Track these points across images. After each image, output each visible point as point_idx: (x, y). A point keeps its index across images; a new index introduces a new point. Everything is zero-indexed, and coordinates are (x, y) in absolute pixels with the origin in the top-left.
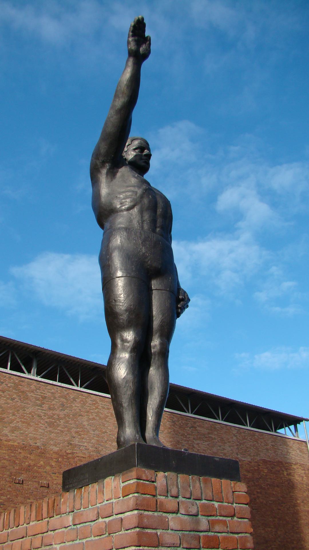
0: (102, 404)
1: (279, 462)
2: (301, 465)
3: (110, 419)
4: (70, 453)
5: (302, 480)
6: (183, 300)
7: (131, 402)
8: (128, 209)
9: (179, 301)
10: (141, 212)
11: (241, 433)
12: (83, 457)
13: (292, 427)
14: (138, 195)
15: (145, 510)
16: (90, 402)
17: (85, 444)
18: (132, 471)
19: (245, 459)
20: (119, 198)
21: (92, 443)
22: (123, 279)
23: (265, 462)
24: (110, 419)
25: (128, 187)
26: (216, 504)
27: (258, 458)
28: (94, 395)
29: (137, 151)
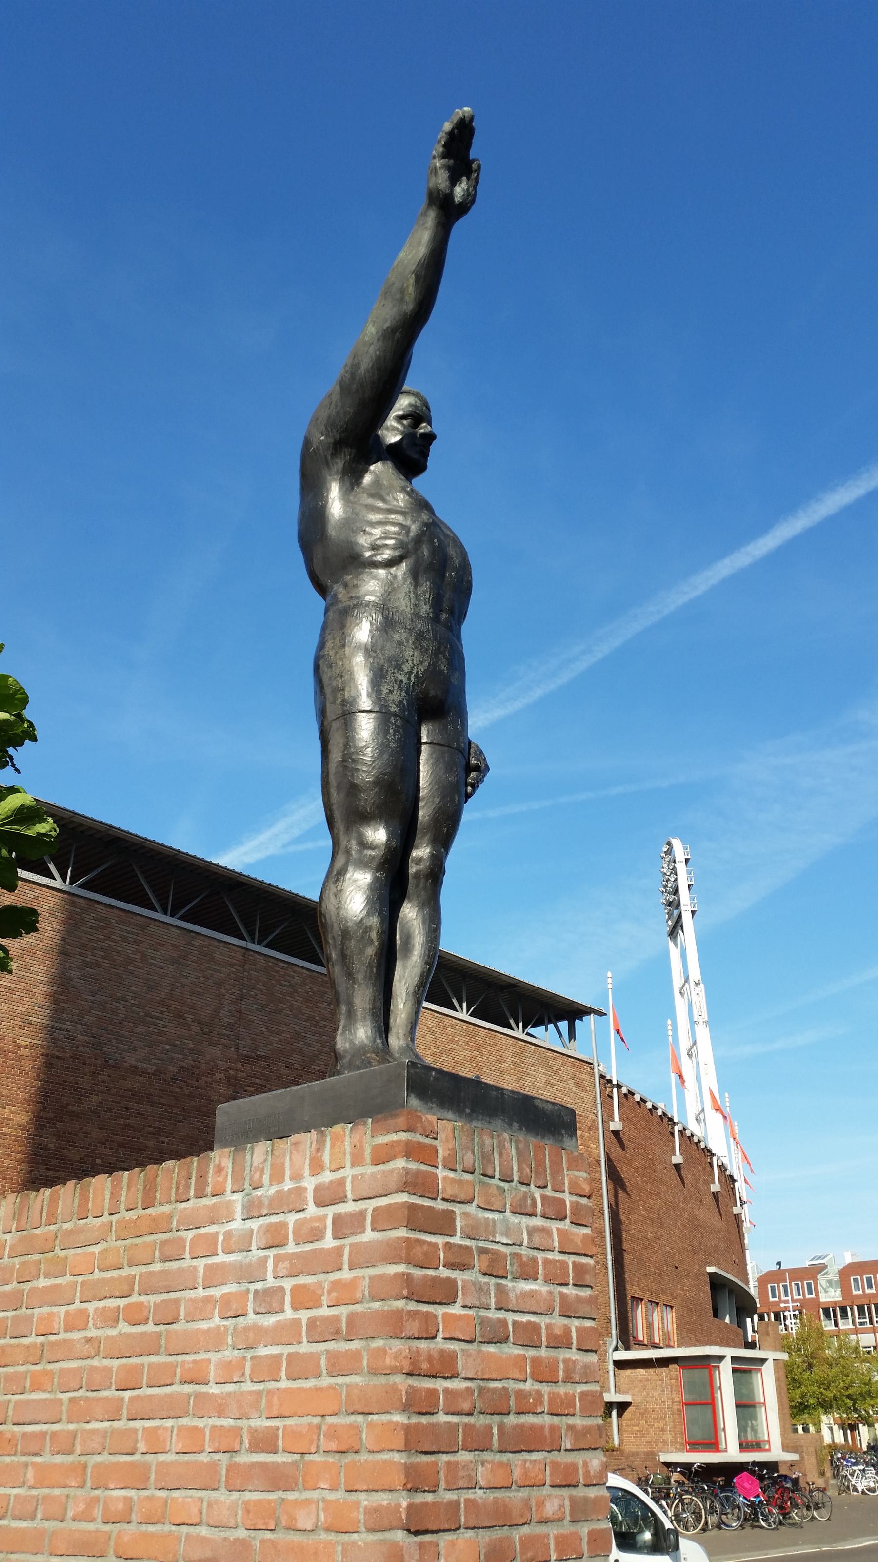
4: (25, 1047)
6: (477, 768)
7: (372, 971)
8: (389, 564)
9: (469, 769)
10: (414, 575)
11: (445, 1028)
12: (58, 1057)
13: (563, 1025)
14: (412, 534)
17: (68, 1026)
20: (370, 534)
22: (373, 715)
25: (390, 511)
28: (105, 905)
29: (405, 422)
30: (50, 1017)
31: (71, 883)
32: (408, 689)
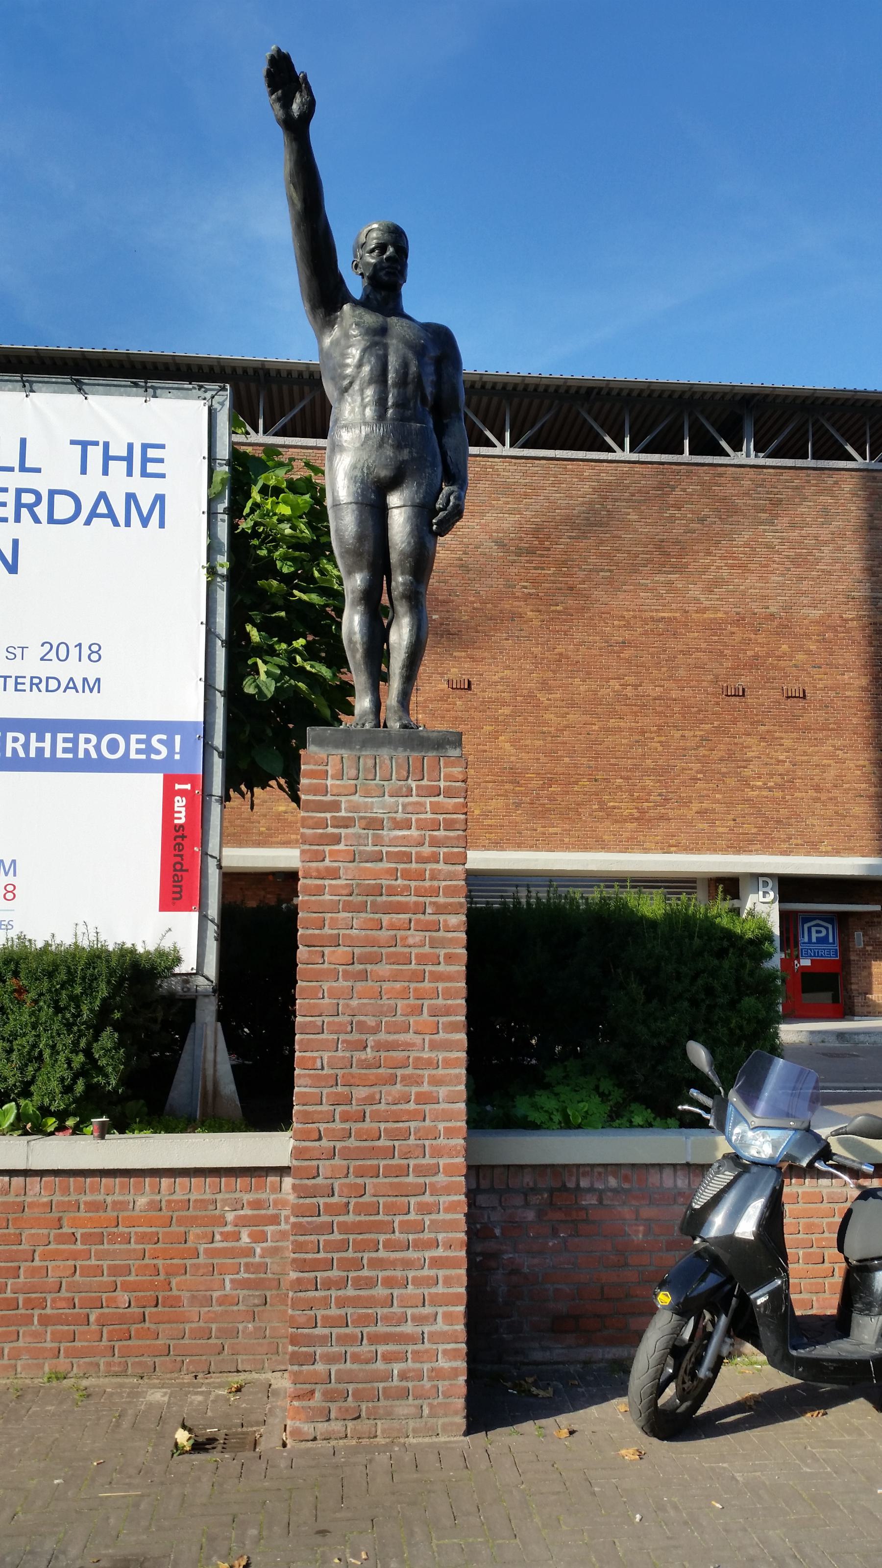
30: (872, 589)
31: (871, 459)
32: (362, 480)
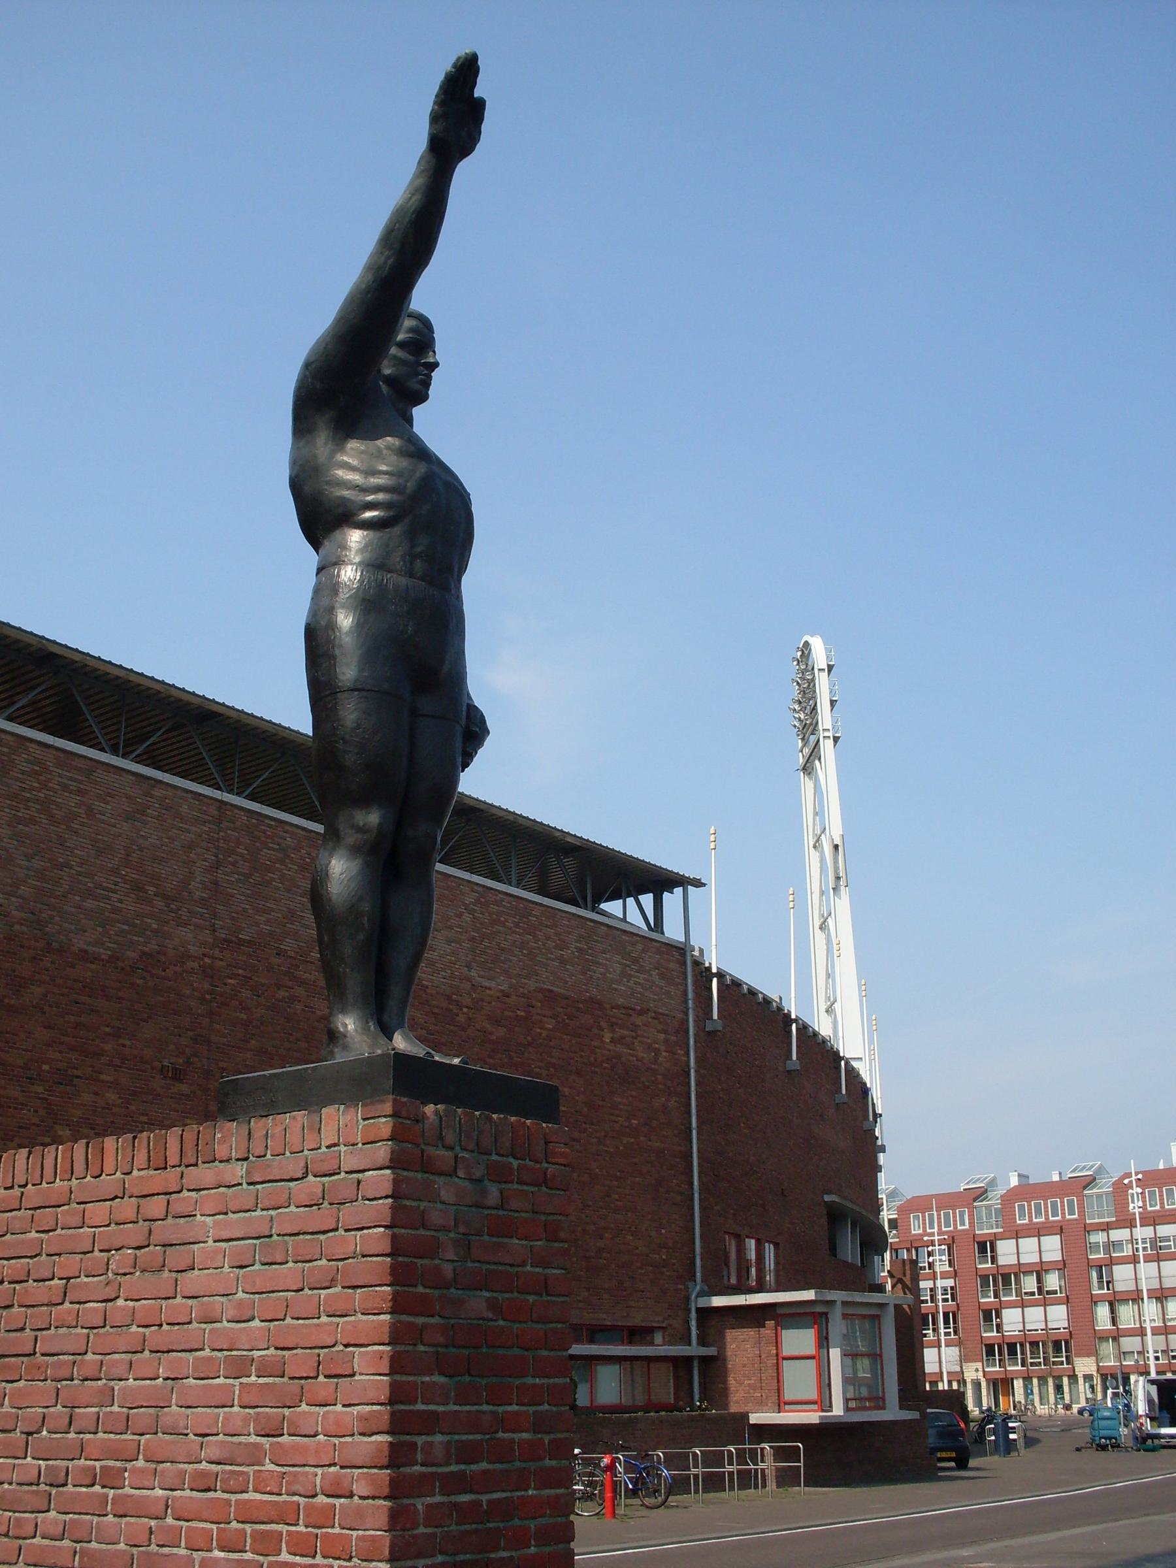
0: (60, 776)
1: (592, 1000)
2: (657, 1016)
3: (82, 824)
5: (655, 1061)
13: (647, 900)
15: (404, 1169)
16: (24, 767)
18: (383, 1101)
19: (492, 984)
21: (20, 897)
23: (550, 997)
24: (82, 824)
26: (515, 1163)
27: (532, 985)
